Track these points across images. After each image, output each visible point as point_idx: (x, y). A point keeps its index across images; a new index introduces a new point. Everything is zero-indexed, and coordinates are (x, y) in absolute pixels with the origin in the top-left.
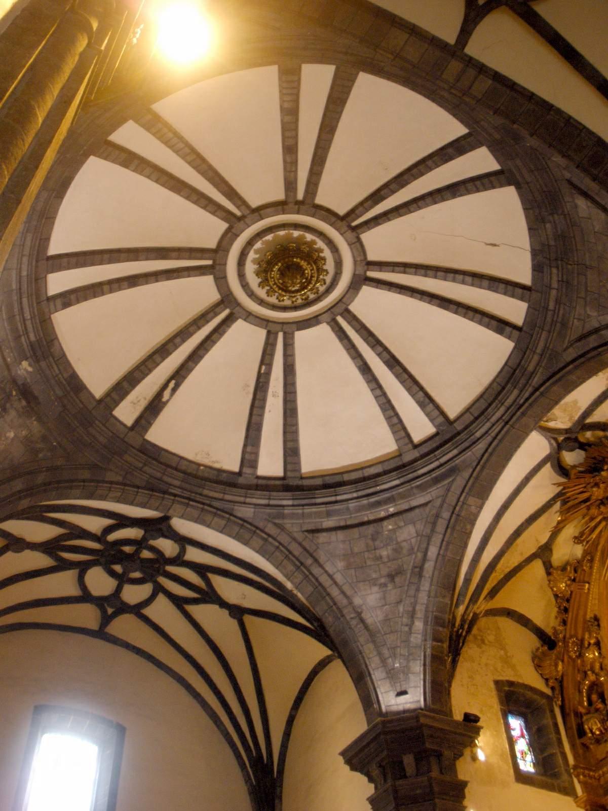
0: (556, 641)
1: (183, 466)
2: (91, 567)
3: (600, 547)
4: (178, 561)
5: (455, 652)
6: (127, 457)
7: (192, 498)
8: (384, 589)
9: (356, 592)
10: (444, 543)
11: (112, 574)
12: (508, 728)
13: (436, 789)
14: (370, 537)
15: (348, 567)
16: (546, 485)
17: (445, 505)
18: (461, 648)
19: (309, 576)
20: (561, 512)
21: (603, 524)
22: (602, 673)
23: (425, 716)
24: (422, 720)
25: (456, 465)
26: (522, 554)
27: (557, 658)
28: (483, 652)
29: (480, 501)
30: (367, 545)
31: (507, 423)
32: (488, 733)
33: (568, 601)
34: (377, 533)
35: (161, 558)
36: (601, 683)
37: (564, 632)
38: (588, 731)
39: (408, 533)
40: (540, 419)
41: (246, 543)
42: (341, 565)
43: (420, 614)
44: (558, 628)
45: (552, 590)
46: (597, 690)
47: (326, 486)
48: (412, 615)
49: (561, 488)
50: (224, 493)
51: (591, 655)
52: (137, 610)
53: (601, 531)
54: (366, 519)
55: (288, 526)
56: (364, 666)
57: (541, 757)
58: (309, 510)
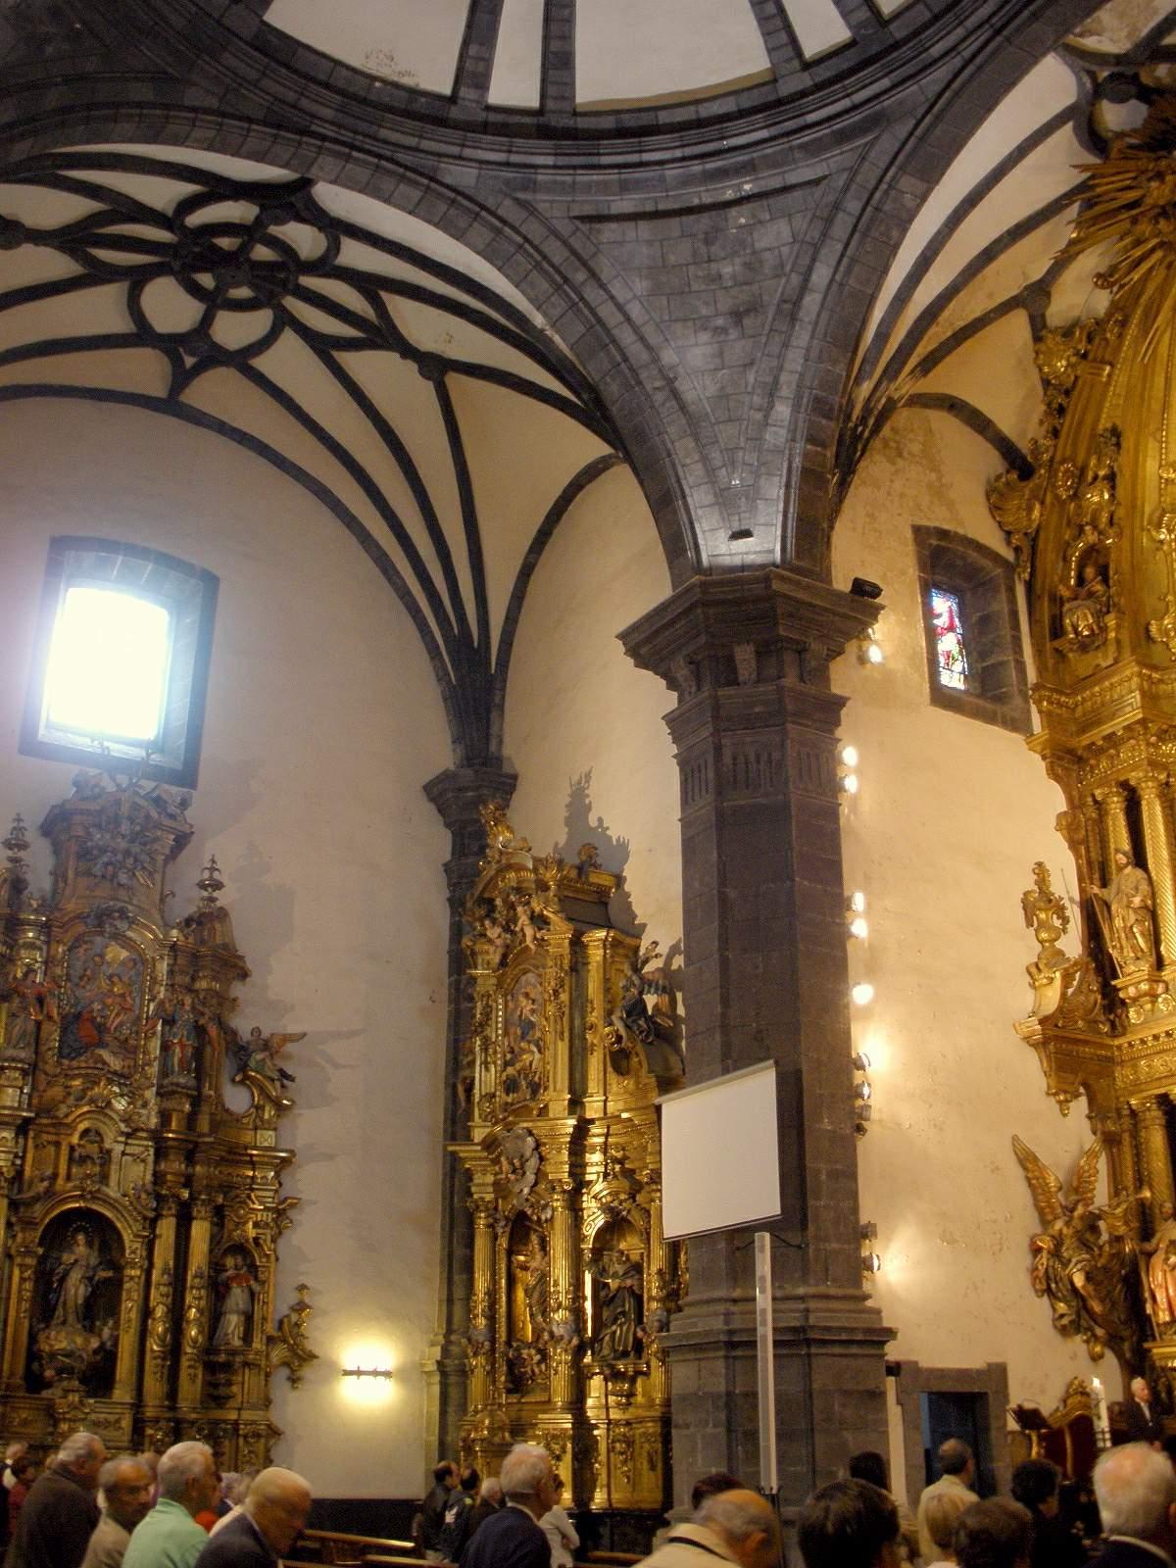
0: (1035, 465)
1: (340, 79)
2: (152, 279)
3: (1143, 300)
4: (324, 266)
5: (847, 466)
6: (228, 59)
7: (358, 143)
8: (722, 337)
9: (667, 340)
10: (845, 260)
11: (195, 290)
12: (929, 614)
13: (790, 707)
14: (701, 236)
15: (656, 291)
16: (1057, 167)
17: (854, 186)
18: (858, 461)
19: (578, 305)
20: (1079, 224)
21: (1159, 254)
22: (1111, 531)
23: (782, 578)
24: (776, 585)
25: (883, 109)
26: (991, 295)
27: (1034, 497)
28: (897, 471)
29: (922, 186)
30: (695, 253)
31: (998, 32)
32: (892, 618)
33: (1067, 393)
34: (717, 230)
35: (291, 262)
36: (1108, 548)
37: (1052, 450)
38: (1070, 629)
39: (775, 235)
40: (1068, 31)
41: (459, 235)
42: (641, 286)
43: (786, 391)
44: (1042, 441)
45: (1041, 370)
46: (1096, 562)
47: (622, 133)
48: (772, 392)
49: (1086, 175)
50: (421, 137)
51: (1097, 496)
52: (242, 360)
53: (1151, 269)
54: (696, 201)
55: (541, 207)
56: (673, 480)
57: (979, 666)
58: (586, 178)
